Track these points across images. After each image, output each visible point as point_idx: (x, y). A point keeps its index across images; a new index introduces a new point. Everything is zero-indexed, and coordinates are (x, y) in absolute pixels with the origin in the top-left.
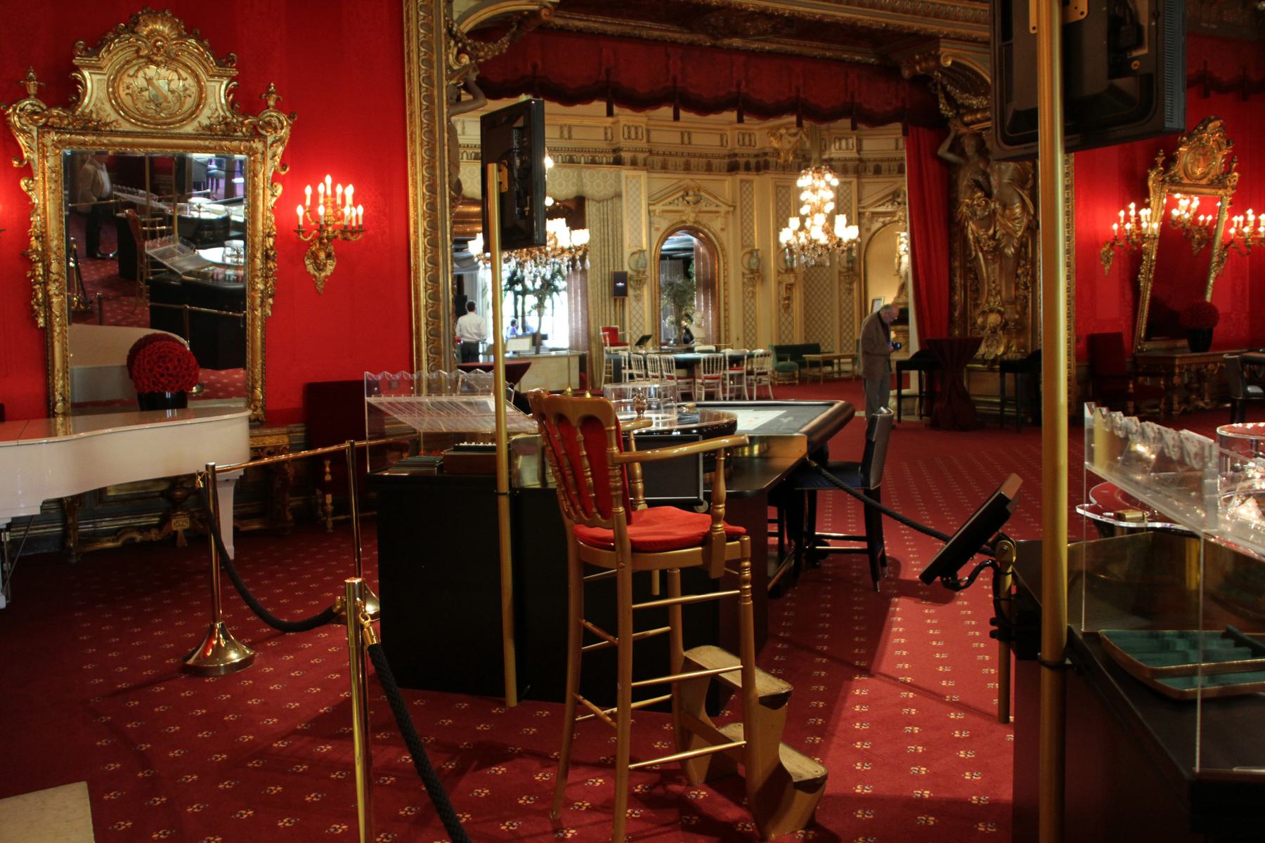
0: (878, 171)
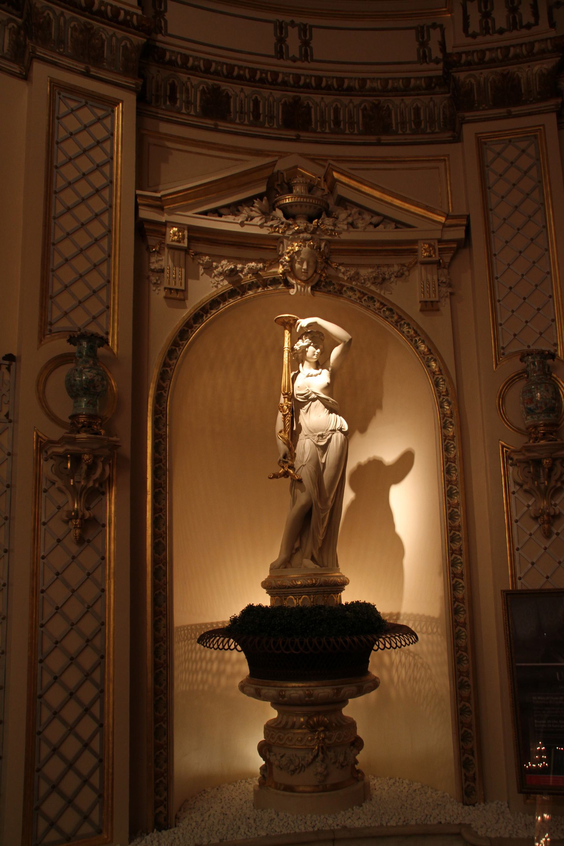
0: (215, 107)
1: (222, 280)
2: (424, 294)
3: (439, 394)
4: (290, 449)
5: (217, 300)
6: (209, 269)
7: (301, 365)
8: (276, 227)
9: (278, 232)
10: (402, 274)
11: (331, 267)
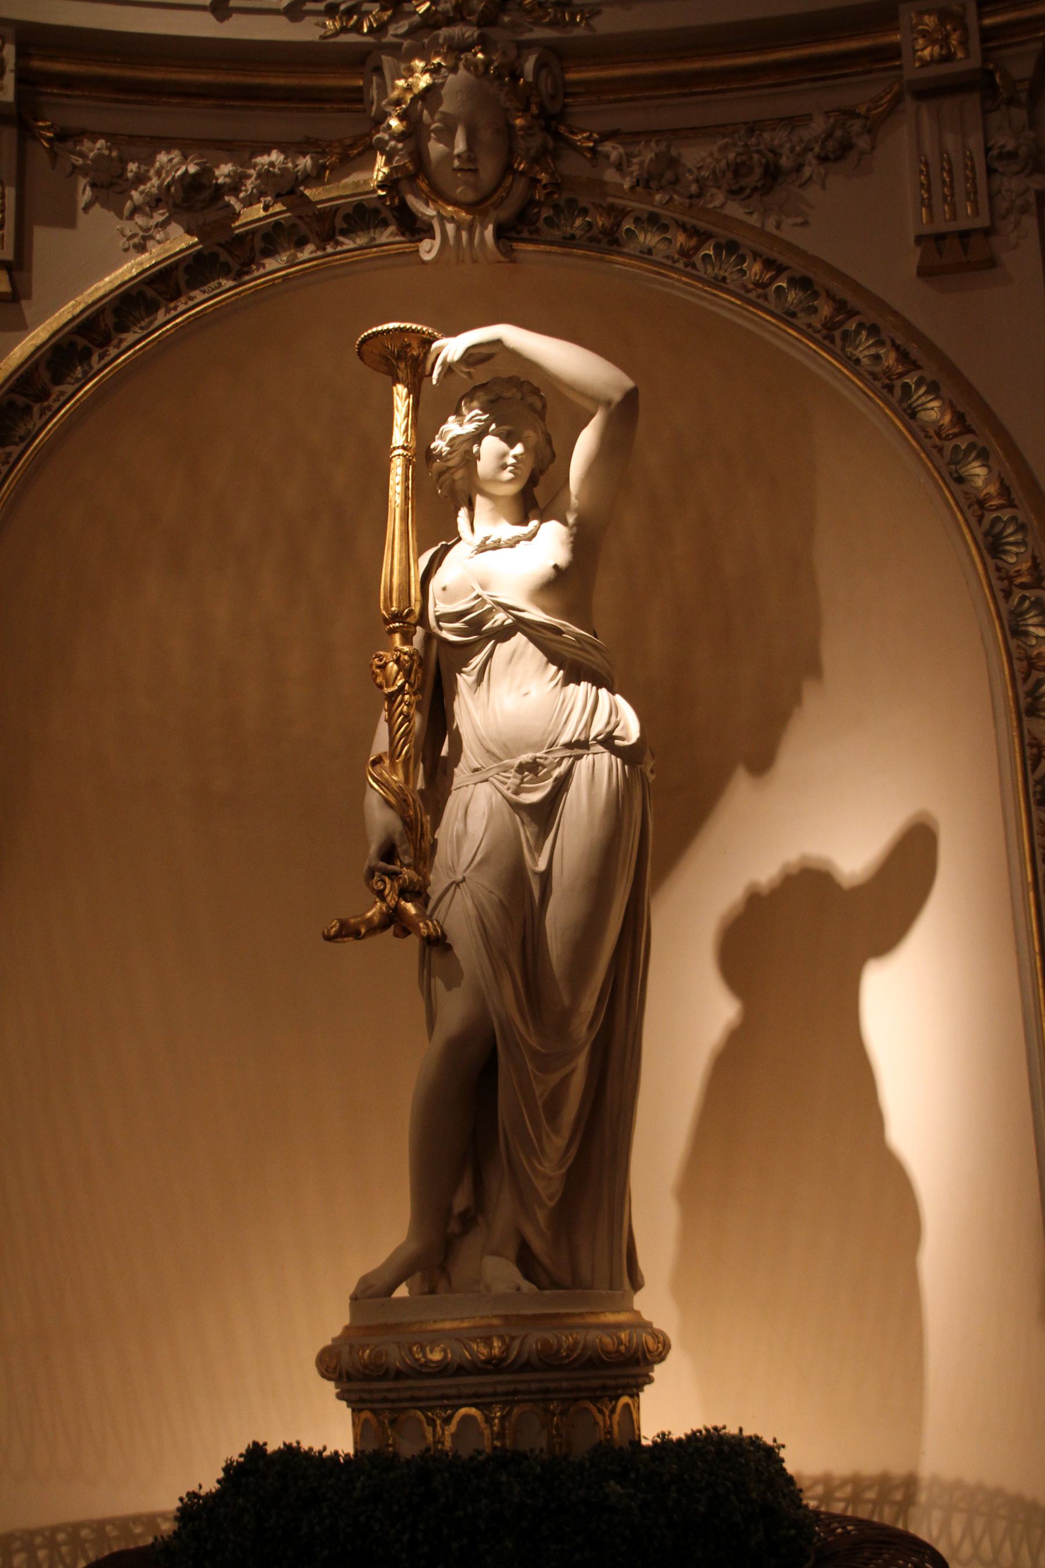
1: (163, 225)
2: (929, 207)
3: (1004, 584)
4: (410, 825)
5: (141, 294)
6: (111, 187)
7: (463, 513)
8: (349, 13)
9: (357, 28)
10: (846, 147)
11: (571, 145)
